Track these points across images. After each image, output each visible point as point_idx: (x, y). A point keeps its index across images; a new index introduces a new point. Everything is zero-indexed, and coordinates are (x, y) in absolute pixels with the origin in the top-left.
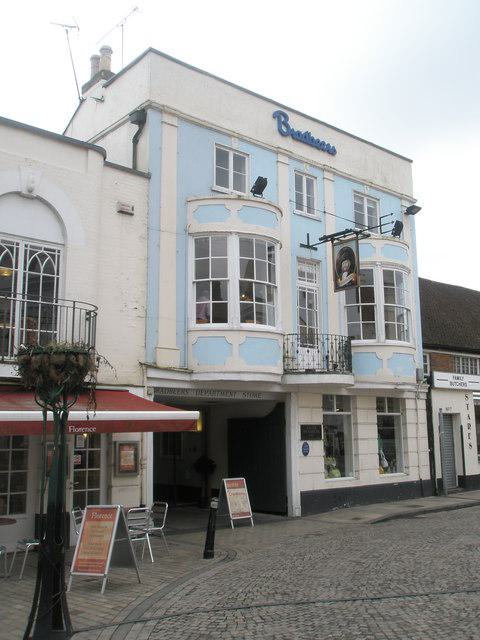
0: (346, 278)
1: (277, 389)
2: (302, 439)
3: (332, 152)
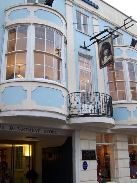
0: (106, 59)
1: (65, 127)
2: (83, 159)
3: (97, 8)
